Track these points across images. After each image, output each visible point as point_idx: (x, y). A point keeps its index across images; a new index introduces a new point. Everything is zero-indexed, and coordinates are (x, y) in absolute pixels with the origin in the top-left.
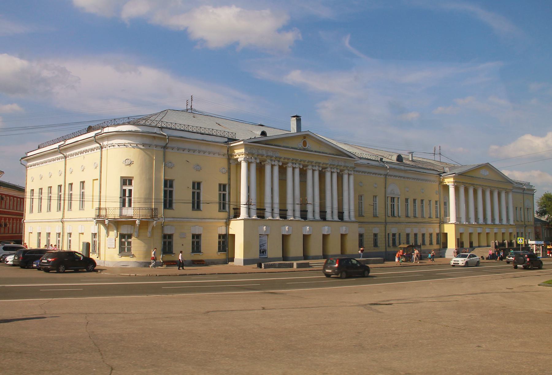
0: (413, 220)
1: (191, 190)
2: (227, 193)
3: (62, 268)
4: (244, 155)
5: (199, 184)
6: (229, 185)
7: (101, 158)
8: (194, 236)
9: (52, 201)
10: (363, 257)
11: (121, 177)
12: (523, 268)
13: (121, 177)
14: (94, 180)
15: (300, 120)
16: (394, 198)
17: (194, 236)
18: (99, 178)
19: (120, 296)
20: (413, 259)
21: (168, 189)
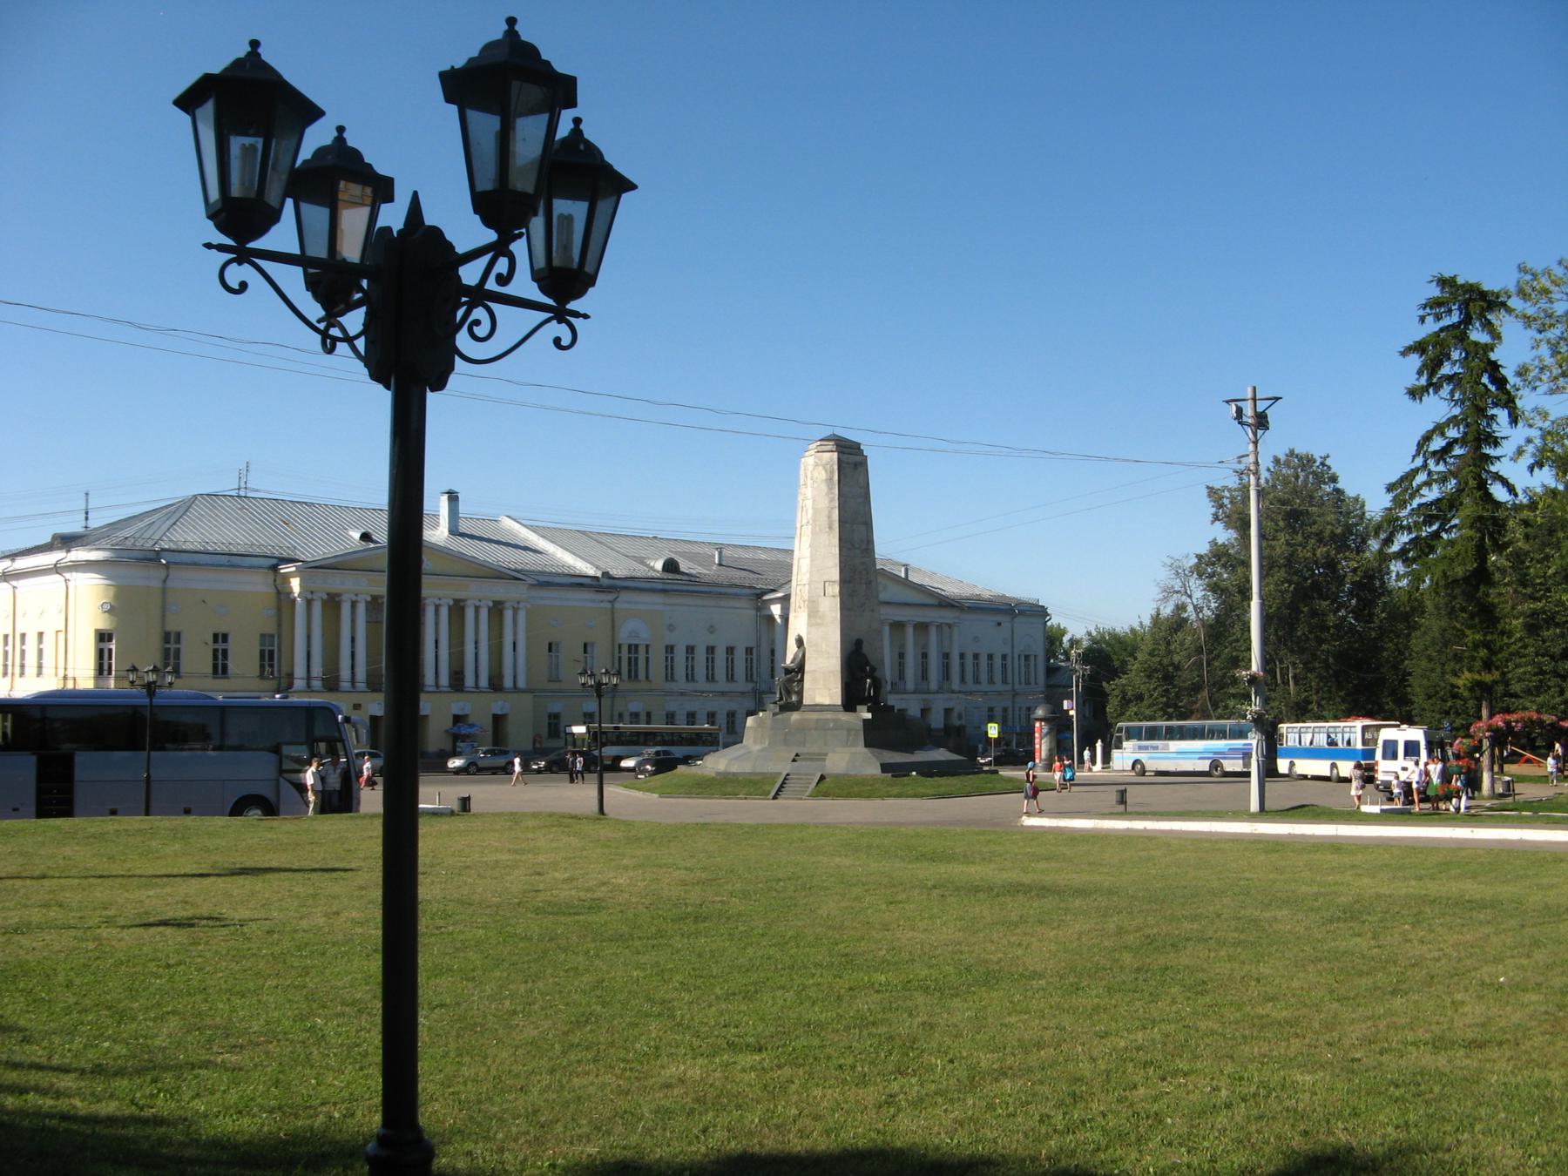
0: (985, 686)
1: (211, 646)
2: (276, 649)
3: (554, 769)
4: (1283, 570)
5: (225, 638)
6: (279, 636)
7: (67, 598)
8: (550, 716)
9: (305, 675)
10: (1523, 755)
11: (97, 631)
12: (1099, 745)
13: (97, 631)
14: (57, 632)
15: (457, 498)
16: (637, 646)
17: (550, 716)
18: (63, 629)
19: (1521, 842)
20: (1245, 745)
21: (220, 646)
